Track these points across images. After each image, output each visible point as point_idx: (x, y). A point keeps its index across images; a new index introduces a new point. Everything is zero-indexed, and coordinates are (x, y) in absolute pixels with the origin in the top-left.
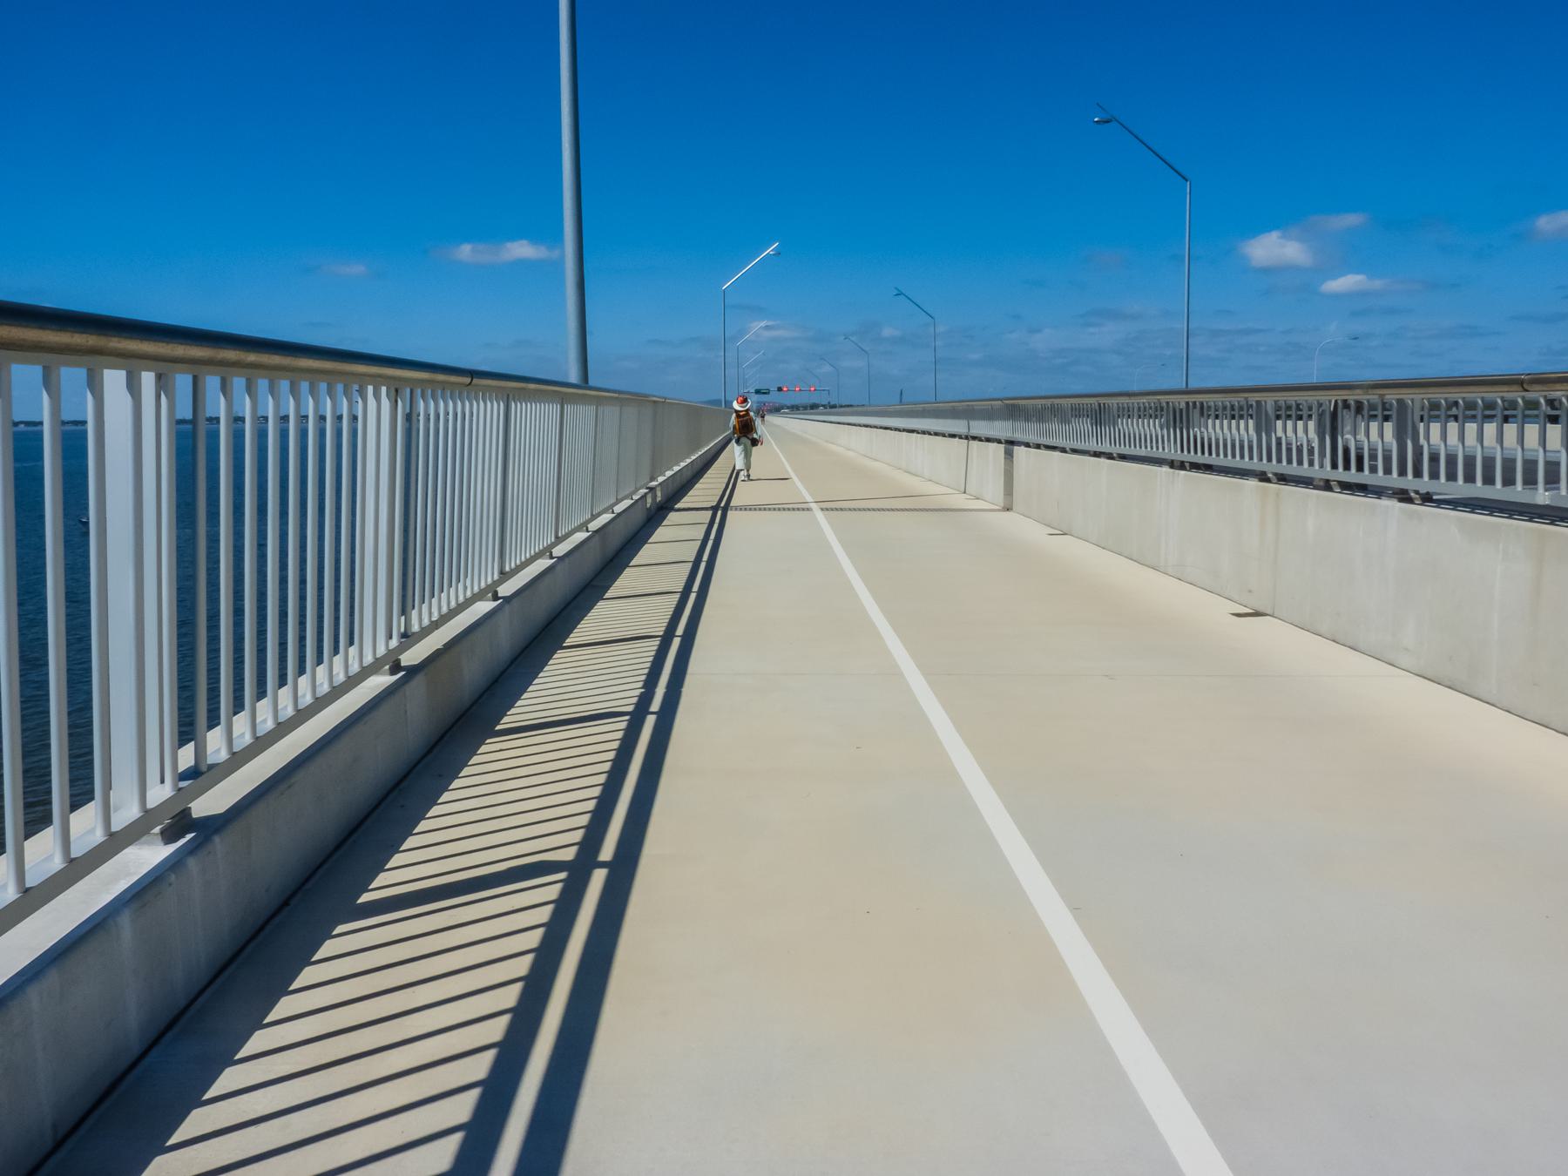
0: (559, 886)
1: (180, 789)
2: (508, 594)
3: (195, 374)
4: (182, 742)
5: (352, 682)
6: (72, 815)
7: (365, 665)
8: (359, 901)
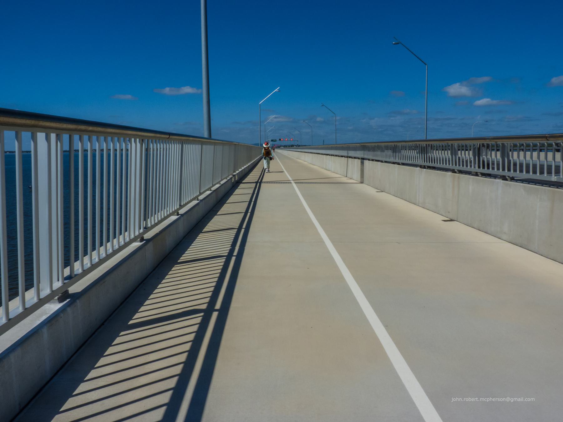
0: (201, 318)
1: (64, 283)
2: (182, 213)
4: (65, 266)
5: (126, 245)
6: (64, 269)
7: (131, 238)
8: (129, 323)
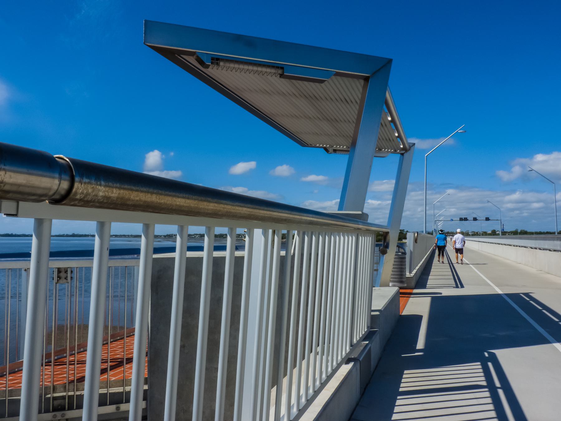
3: (288, 230)
